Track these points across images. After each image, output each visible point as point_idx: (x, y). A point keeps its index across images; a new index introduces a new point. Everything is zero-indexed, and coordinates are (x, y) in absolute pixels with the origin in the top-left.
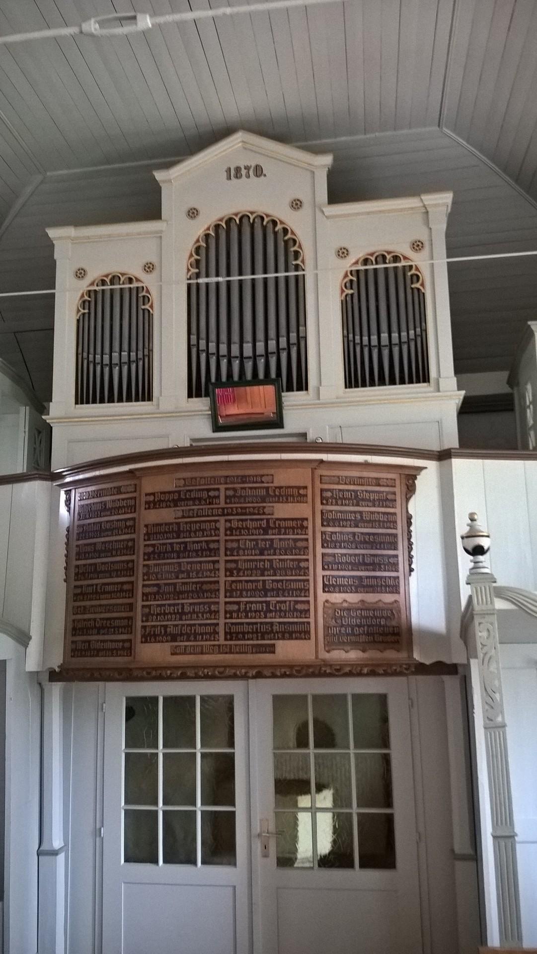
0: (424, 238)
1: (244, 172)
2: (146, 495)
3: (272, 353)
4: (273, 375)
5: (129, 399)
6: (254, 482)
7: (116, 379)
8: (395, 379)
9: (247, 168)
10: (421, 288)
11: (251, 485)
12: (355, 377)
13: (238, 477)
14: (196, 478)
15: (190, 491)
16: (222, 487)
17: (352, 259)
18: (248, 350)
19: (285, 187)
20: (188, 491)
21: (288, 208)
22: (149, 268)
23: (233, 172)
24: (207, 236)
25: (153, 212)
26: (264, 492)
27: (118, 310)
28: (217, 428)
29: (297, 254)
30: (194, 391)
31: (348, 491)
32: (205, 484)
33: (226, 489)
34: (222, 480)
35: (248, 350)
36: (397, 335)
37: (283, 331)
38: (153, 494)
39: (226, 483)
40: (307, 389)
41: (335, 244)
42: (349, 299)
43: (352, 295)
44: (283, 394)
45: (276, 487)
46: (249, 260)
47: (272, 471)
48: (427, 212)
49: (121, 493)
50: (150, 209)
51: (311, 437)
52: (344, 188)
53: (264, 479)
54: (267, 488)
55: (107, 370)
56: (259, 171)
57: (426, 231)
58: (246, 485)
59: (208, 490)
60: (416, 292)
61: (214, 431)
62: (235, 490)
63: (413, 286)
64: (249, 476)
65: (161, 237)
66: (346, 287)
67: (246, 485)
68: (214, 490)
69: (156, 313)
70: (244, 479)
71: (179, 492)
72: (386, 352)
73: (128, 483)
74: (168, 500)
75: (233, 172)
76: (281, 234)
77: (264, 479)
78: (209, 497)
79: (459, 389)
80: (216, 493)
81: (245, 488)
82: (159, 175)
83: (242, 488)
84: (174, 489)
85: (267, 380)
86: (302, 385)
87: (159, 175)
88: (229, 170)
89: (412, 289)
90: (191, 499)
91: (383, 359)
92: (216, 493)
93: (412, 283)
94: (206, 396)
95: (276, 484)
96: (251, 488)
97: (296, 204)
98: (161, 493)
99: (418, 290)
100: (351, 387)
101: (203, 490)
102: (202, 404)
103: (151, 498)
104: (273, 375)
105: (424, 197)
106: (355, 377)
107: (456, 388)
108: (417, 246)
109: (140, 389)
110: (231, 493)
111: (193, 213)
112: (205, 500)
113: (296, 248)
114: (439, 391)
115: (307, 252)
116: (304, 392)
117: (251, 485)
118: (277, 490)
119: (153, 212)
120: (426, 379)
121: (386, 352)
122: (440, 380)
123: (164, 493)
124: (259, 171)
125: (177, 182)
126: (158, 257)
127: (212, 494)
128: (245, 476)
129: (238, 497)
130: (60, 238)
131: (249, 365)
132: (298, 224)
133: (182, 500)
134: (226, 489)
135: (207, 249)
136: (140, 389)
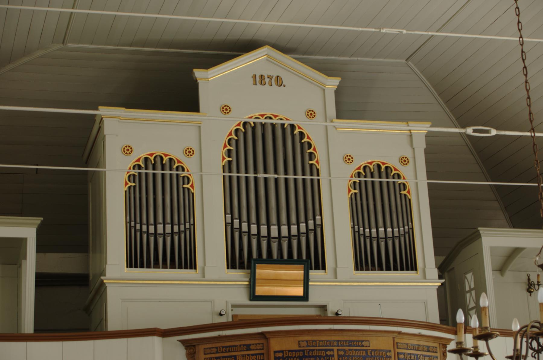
0: (409, 155)
1: (267, 80)
2: (275, 352)
3: (253, 235)
4: (304, 257)
5: (173, 267)
6: (357, 346)
7: (164, 248)
8: (319, 265)
9: (270, 77)
10: (190, 188)
11: (355, 348)
12: (363, 262)
13: (346, 341)
14: (316, 341)
15: (313, 350)
16: (335, 348)
17: (399, 166)
18: (274, 232)
19: (299, 99)
20: (310, 350)
21: (304, 117)
22: (189, 152)
23: (258, 79)
24: (237, 131)
25: (192, 105)
26: (364, 354)
27: (160, 187)
28: (253, 297)
29: (311, 156)
30: (232, 264)
31: (413, 354)
32: (323, 346)
33: (338, 350)
34: (336, 344)
35: (274, 232)
36: (391, 230)
37: (302, 218)
38: (282, 352)
39: (338, 346)
40: (195, 268)
41: (345, 149)
42: (353, 196)
43: (135, 187)
44: (310, 271)
45: (372, 350)
46: (269, 155)
47: (368, 338)
48: (411, 136)
49: (251, 350)
50: (187, 100)
51: (332, 309)
52: (348, 106)
53: (363, 343)
54: (366, 351)
55: (152, 239)
56: (279, 82)
57: (411, 151)
58: (351, 348)
59: (326, 350)
60: (403, 196)
61: (251, 300)
62: (344, 350)
63: (184, 186)
64: (354, 341)
65: (200, 127)
66: (129, 181)
67: (351, 348)
68: (330, 350)
69: (196, 191)
70: (350, 343)
71: (303, 351)
72: (383, 244)
73: (257, 342)
74: (295, 357)
75: (258, 79)
76: (297, 138)
77: (363, 343)
78: (327, 355)
79: (440, 277)
80: (331, 353)
81: (352, 350)
82: (198, 73)
83: (349, 350)
84: (297, 348)
85: (299, 261)
86: (320, 265)
87: (198, 73)
88: (255, 77)
89: (184, 188)
90: (313, 356)
91: (382, 254)
92: (331, 353)
93: (184, 184)
94: (248, 269)
95: (371, 348)
96: (356, 350)
97: (311, 114)
98: (289, 351)
99: (189, 189)
100: (131, 267)
101: (322, 350)
102: (239, 276)
103: (281, 355)
104: (304, 257)
105: (411, 123)
106: (363, 262)
107: (437, 277)
108: (404, 161)
109: (183, 257)
110: (342, 353)
111: (226, 110)
112: (324, 357)
113: (311, 150)
114: (425, 277)
115: (320, 155)
116: (193, 270)
117: (355, 348)
118: (311, 352)
119: (192, 105)
120: (191, 264)
121: (383, 244)
122: (206, 268)
123: (292, 351)
124: (279, 82)
125: (212, 81)
126: (196, 143)
127: (328, 353)
128: (351, 341)
129: (347, 356)
130: (111, 117)
131: (275, 246)
132: (313, 131)
133: (306, 357)
134: (338, 350)
135: (237, 141)
136: (183, 257)
